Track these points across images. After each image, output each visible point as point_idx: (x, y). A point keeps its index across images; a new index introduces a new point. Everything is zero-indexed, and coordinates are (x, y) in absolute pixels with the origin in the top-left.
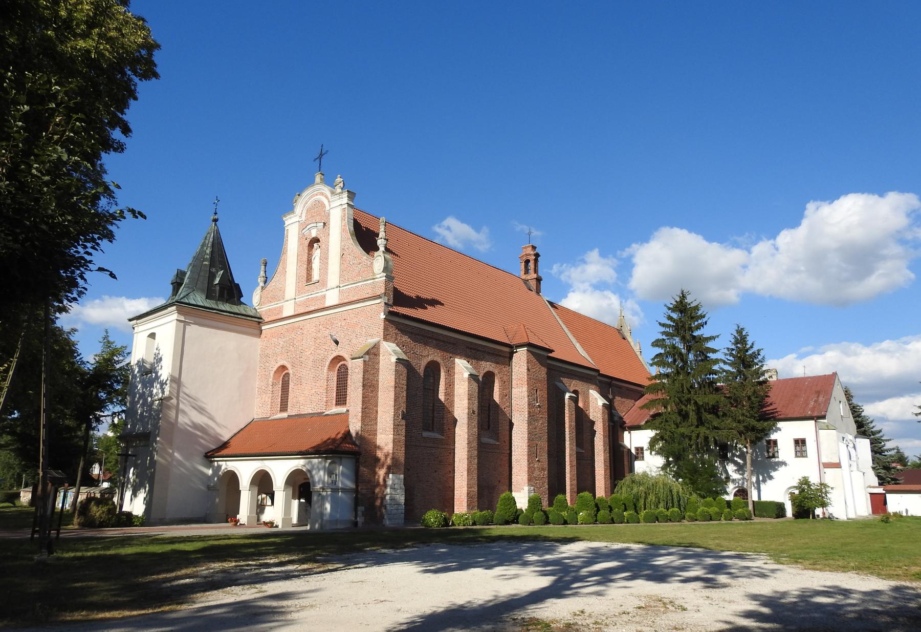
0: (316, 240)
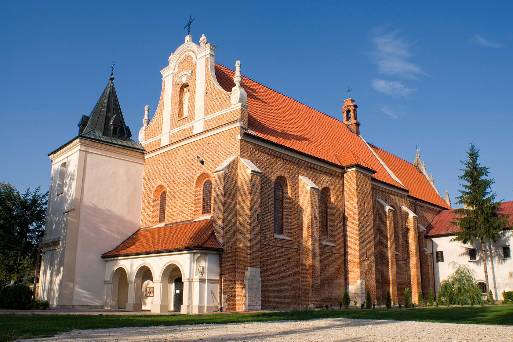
0: (186, 85)
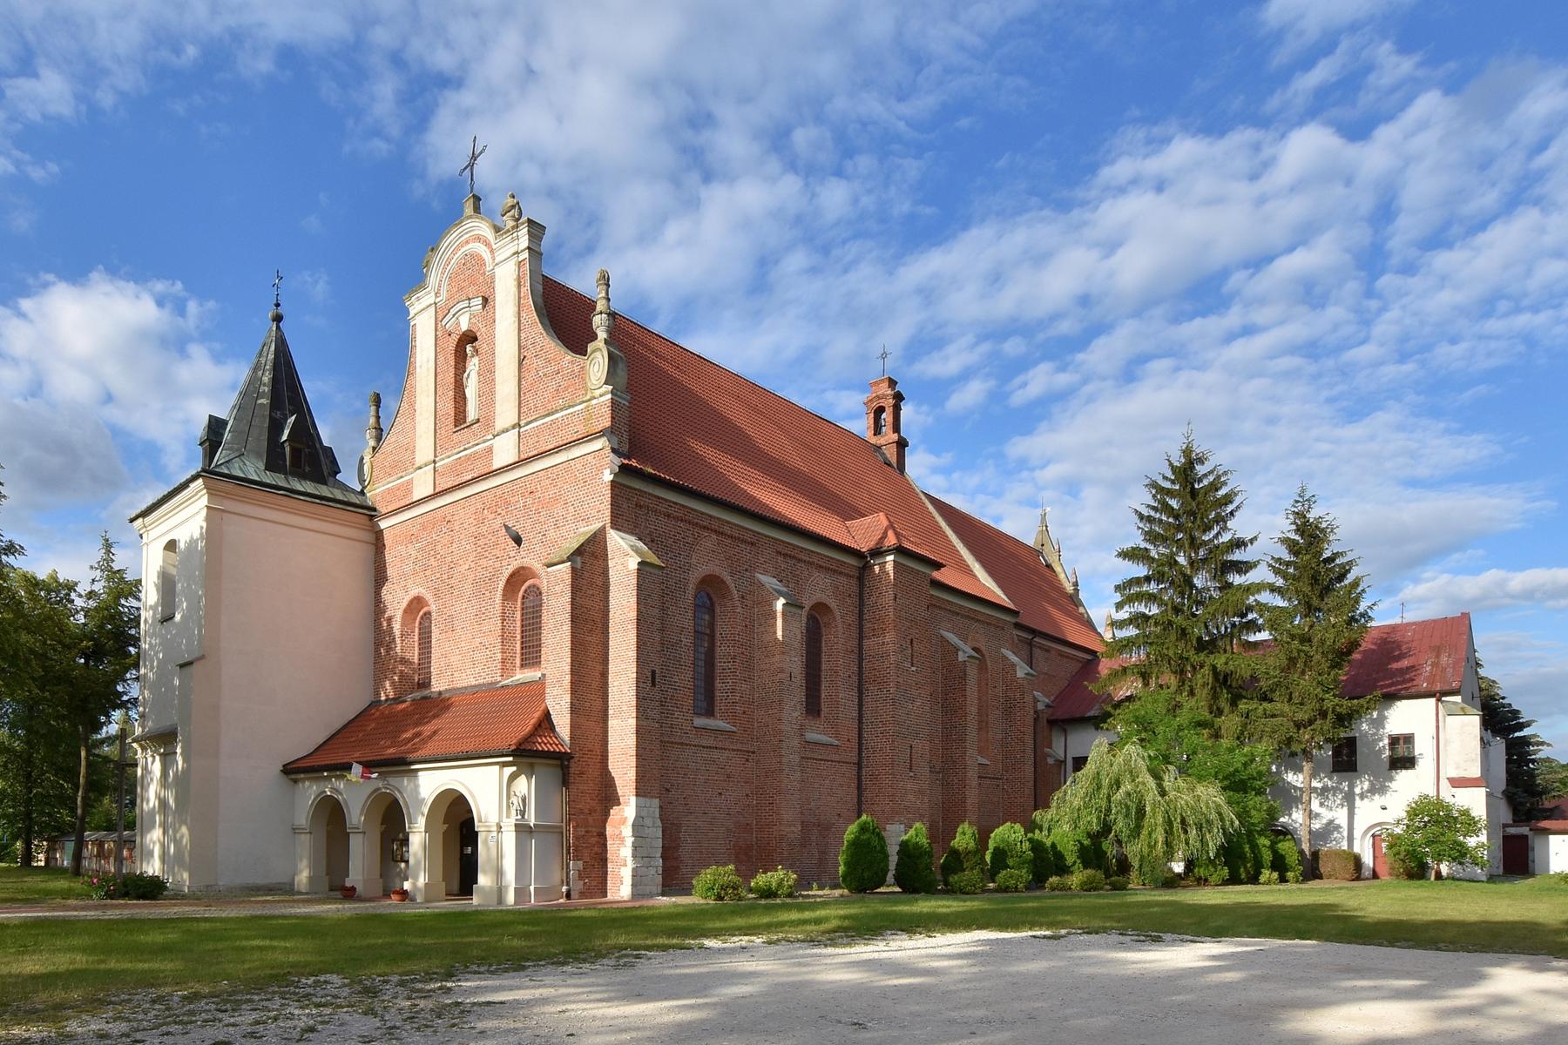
0: (469, 338)
